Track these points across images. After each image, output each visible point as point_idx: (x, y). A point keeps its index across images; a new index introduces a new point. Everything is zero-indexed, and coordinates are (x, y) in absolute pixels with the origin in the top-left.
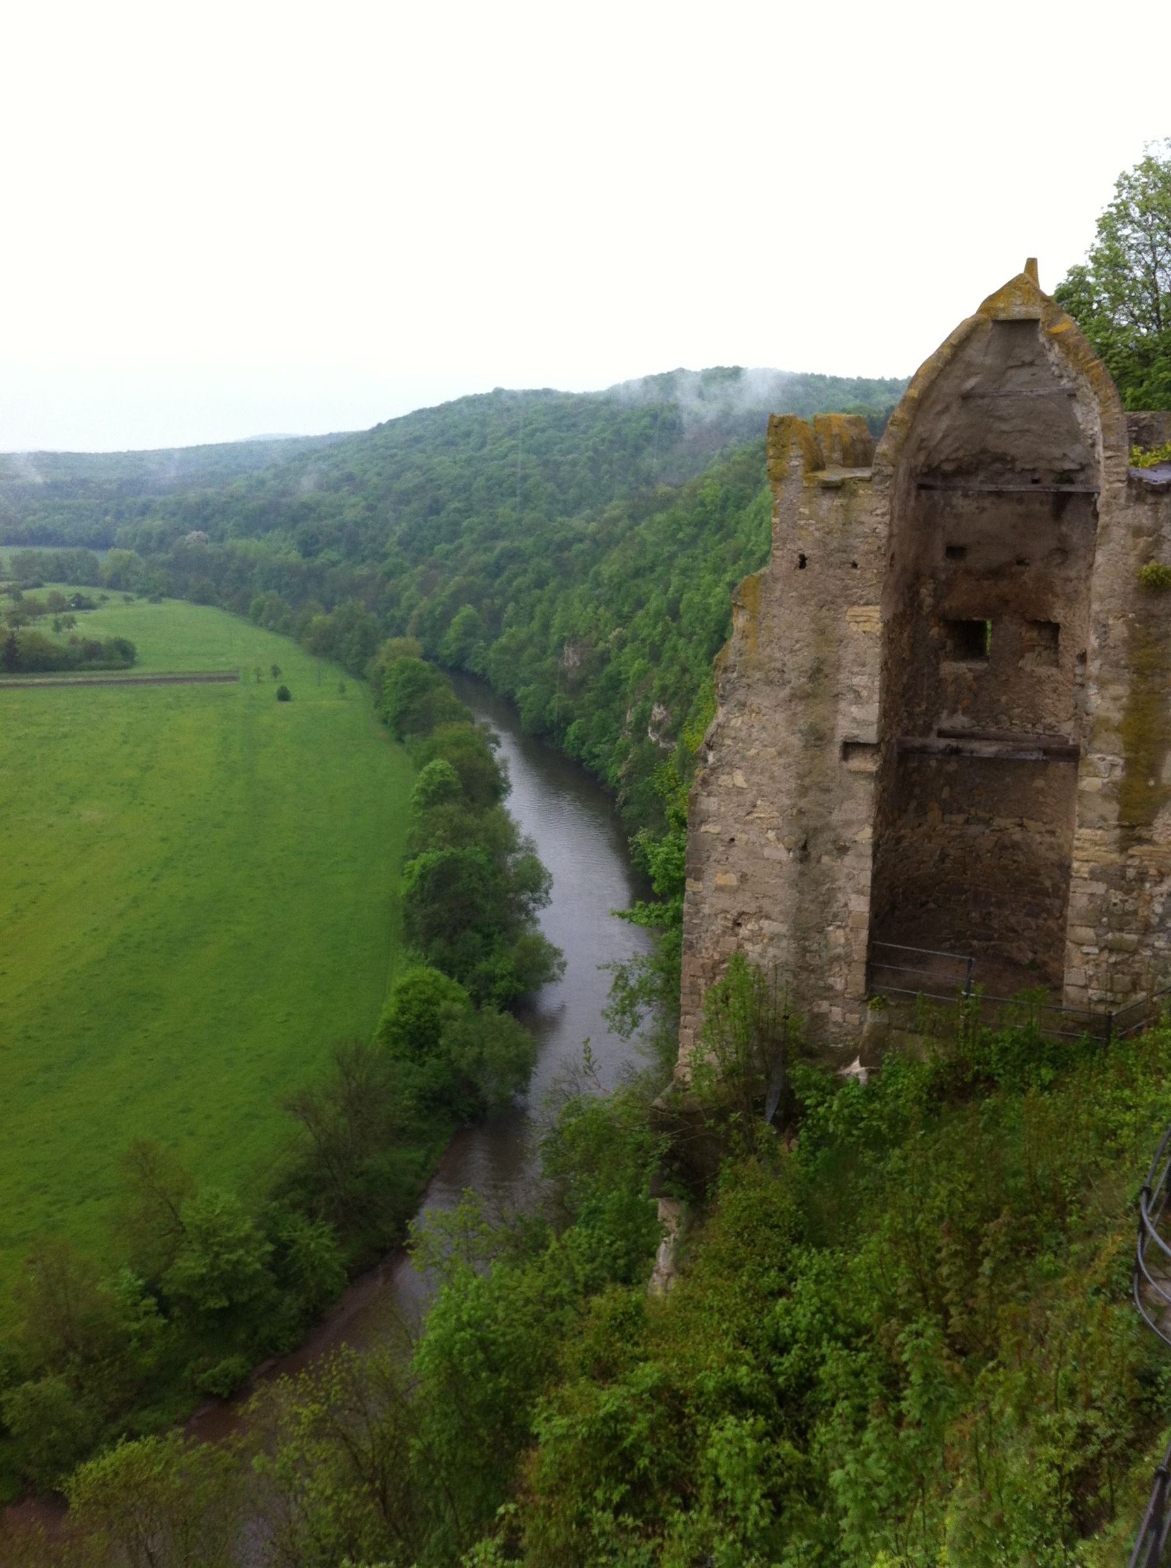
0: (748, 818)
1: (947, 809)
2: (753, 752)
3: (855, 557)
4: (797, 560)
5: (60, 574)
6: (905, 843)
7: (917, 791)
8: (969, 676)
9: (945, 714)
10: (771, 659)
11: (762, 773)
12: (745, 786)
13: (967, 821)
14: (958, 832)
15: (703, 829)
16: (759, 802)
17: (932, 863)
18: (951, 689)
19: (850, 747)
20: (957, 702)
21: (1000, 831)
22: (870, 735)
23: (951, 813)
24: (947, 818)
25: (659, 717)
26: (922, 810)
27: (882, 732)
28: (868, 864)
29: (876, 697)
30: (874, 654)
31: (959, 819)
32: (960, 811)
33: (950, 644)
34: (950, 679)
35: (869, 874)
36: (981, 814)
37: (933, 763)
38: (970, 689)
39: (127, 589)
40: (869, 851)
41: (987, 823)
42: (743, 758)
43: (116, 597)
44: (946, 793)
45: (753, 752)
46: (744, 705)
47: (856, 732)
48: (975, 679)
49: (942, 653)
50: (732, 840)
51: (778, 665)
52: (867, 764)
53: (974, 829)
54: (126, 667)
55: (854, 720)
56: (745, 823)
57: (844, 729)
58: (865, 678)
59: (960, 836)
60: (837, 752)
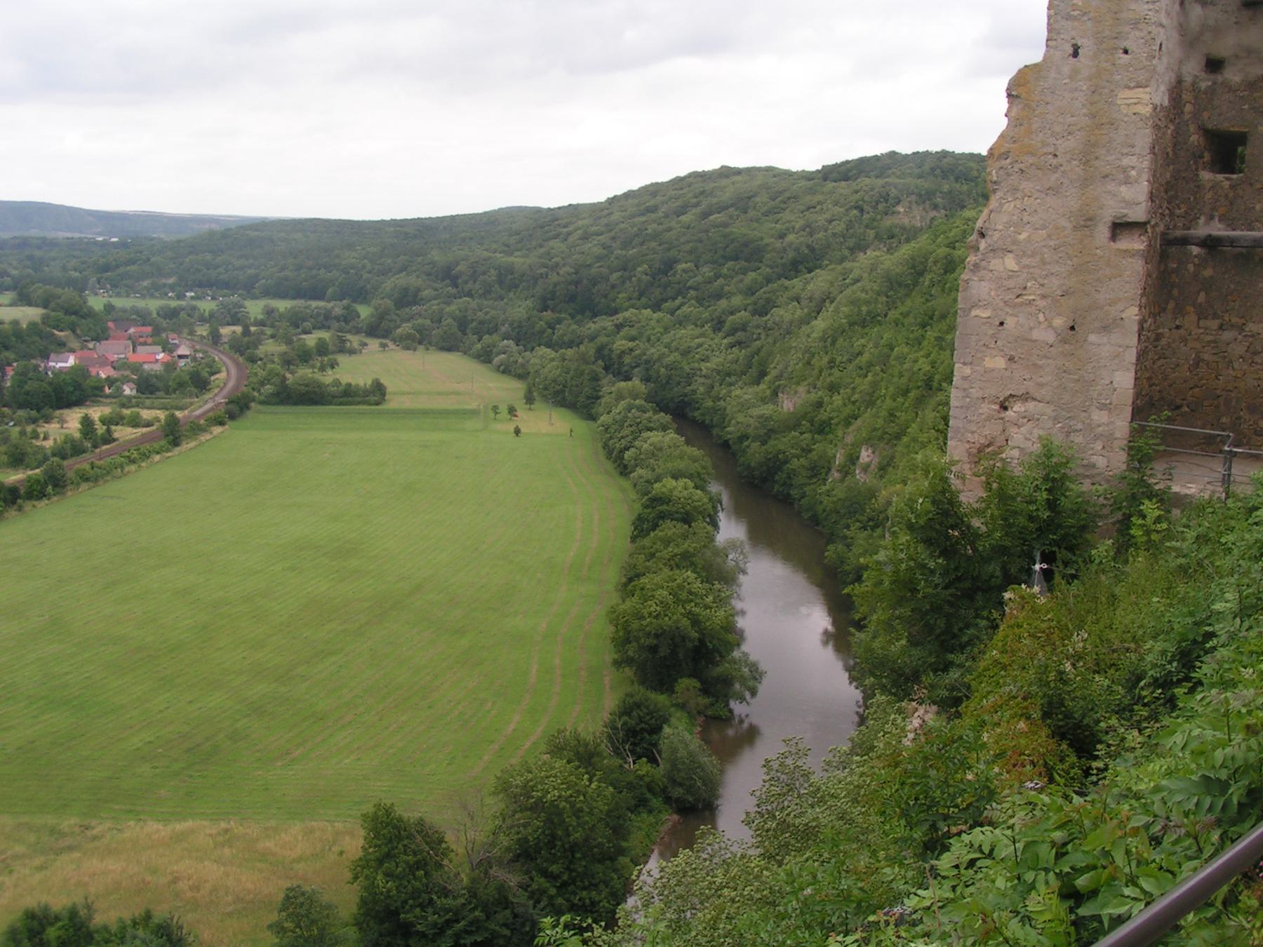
0: (1019, 300)
1: (1201, 316)
2: (1022, 237)
3: (1125, 44)
4: (1071, 51)
5: (323, 321)
6: (1164, 342)
7: (1175, 292)
8: (1226, 184)
9: (1202, 220)
10: (1044, 144)
11: (1032, 256)
12: (1016, 268)
13: (1221, 327)
14: (1211, 338)
15: (974, 313)
16: (1029, 284)
17: (1186, 366)
18: (1208, 196)
19: (1120, 228)
20: (1214, 209)
21: (1252, 336)
22: (1139, 213)
23: (1206, 318)
24: (1202, 323)
25: (867, 460)
26: (1179, 311)
27: (1152, 212)
28: (1134, 340)
29: (1145, 176)
30: (1144, 139)
31: (1214, 324)
32: (1215, 316)
33: (1207, 156)
34: (1208, 186)
35: (1134, 351)
36: (1235, 320)
37: (1191, 267)
38: (1226, 196)
39: (384, 337)
40: (1136, 328)
41: (1241, 328)
42: (1015, 242)
43: (374, 344)
44: (1202, 297)
45: (1022, 237)
46: (1016, 190)
47: (1125, 211)
48: (1232, 187)
49: (1201, 161)
50: (1002, 324)
51: (1051, 149)
52: (1136, 243)
53: (1227, 335)
54: (377, 404)
55: (1123, 201)
56: (1015, 306)
57: (1111, 210)
58: (1134, 158)
59: (1214, 341)
60: (1103, 232)
